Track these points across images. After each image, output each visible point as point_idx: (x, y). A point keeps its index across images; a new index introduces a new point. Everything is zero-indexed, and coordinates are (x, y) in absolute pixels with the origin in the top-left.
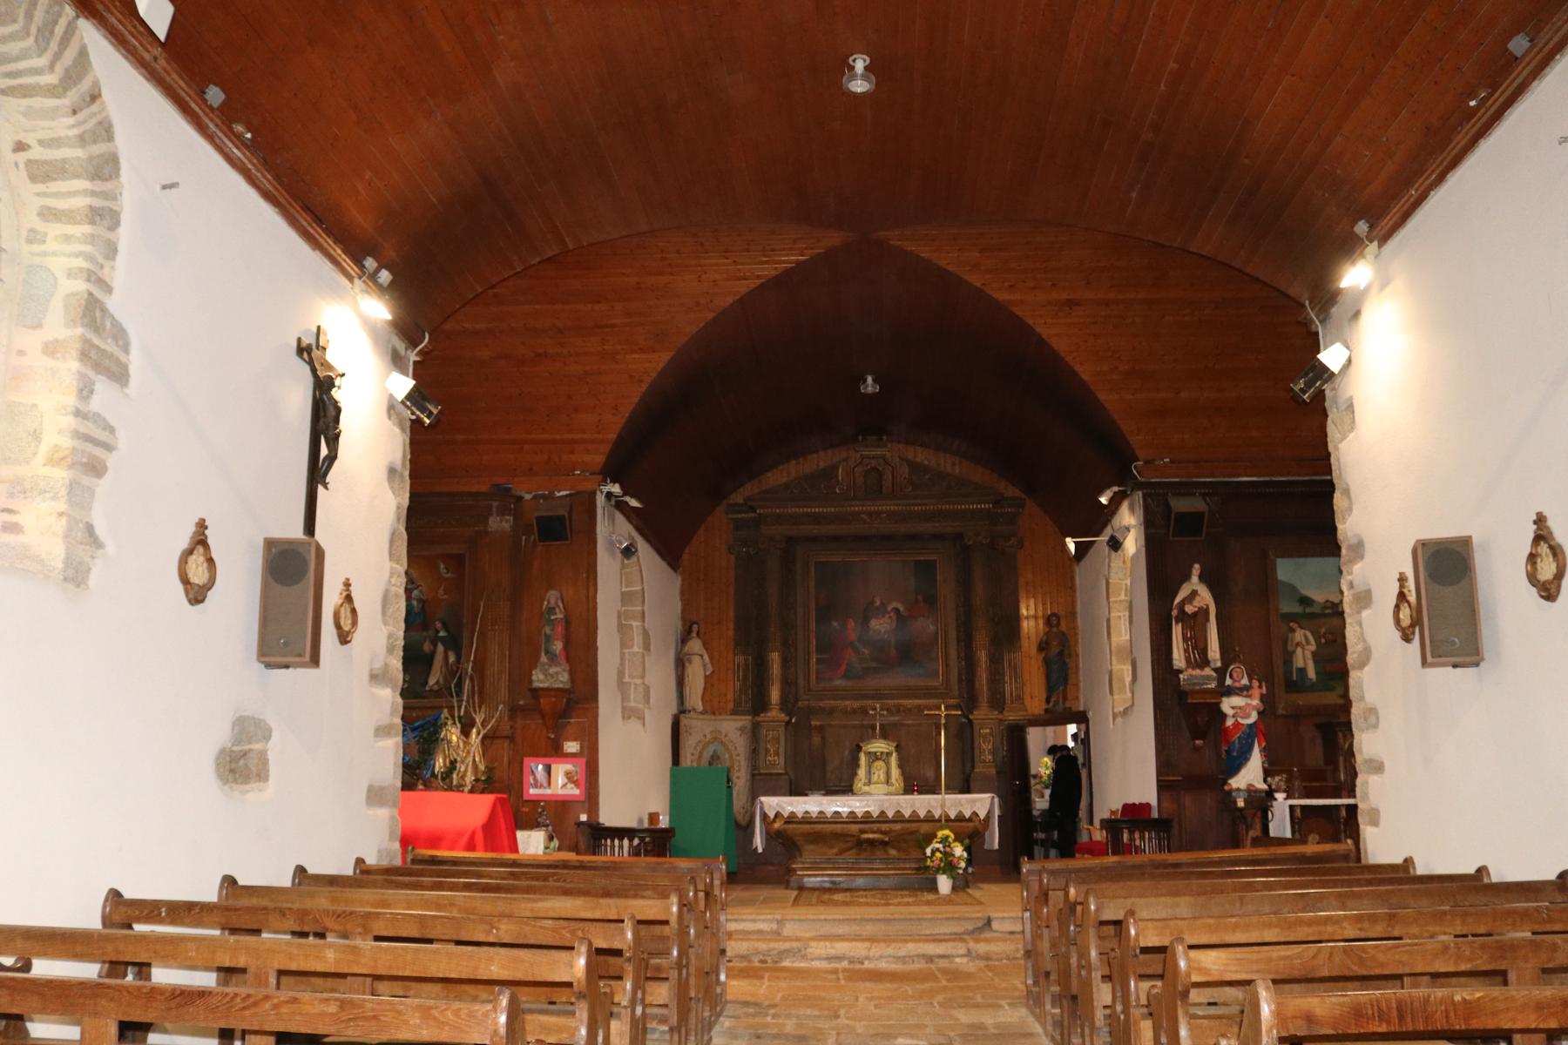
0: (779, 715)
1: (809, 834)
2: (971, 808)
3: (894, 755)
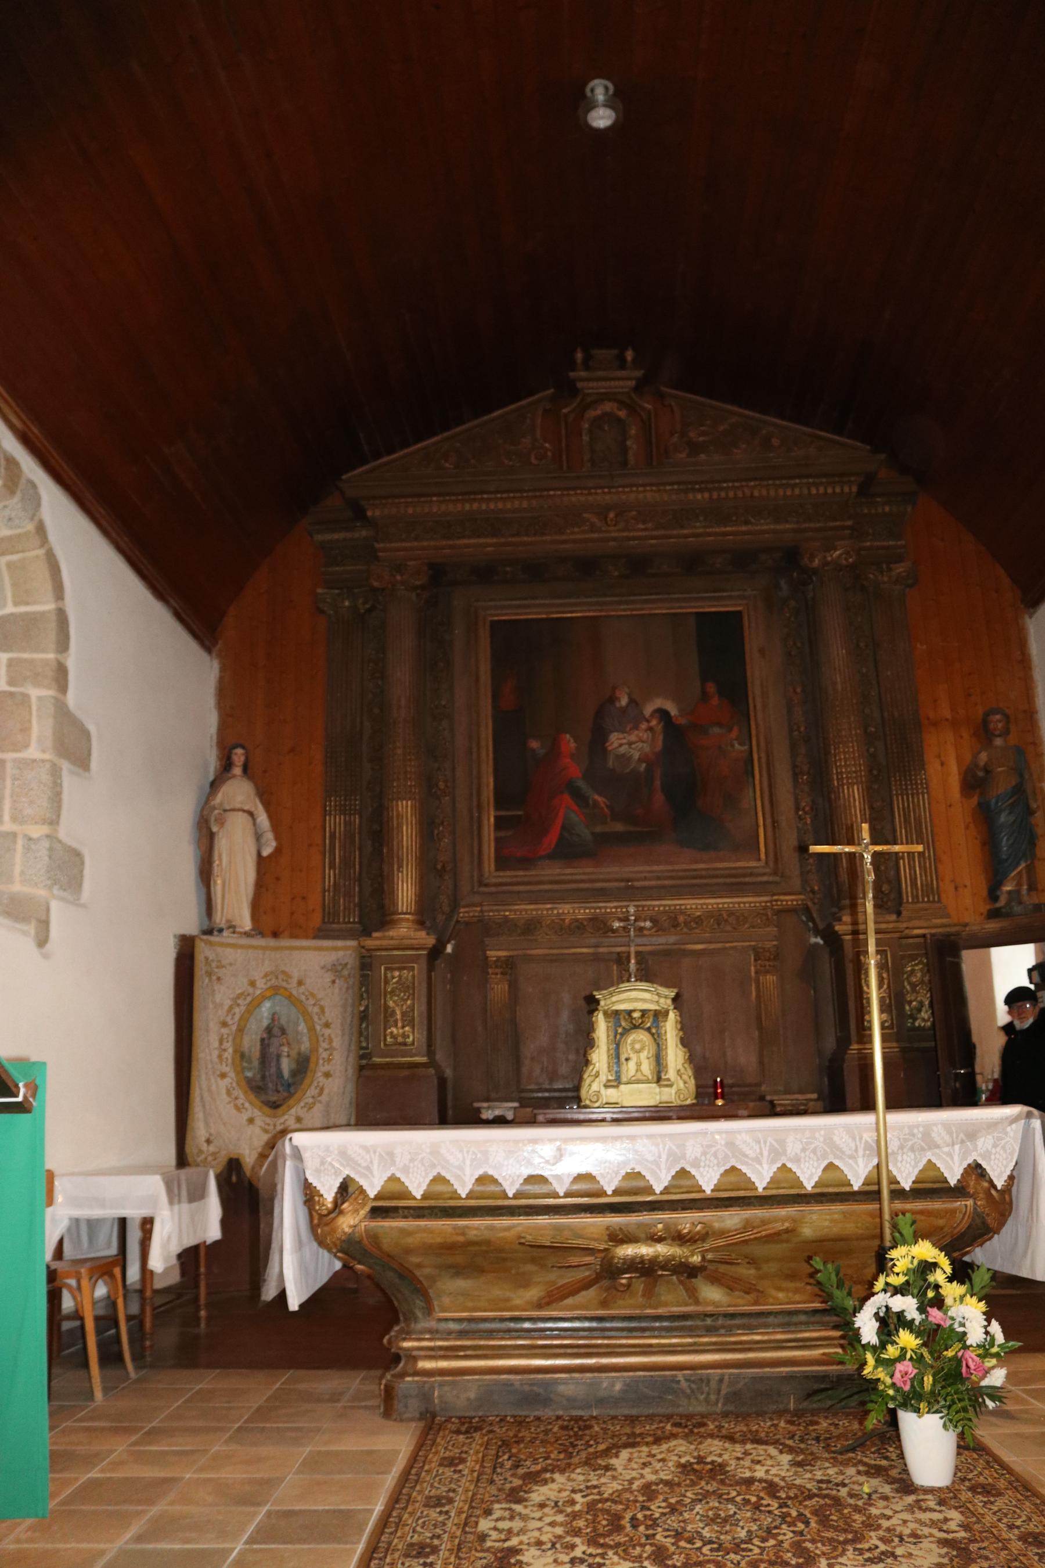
0: (412, 934)
1: (450, 1248)
2: (963, 1157)
3: (672, 1015)
